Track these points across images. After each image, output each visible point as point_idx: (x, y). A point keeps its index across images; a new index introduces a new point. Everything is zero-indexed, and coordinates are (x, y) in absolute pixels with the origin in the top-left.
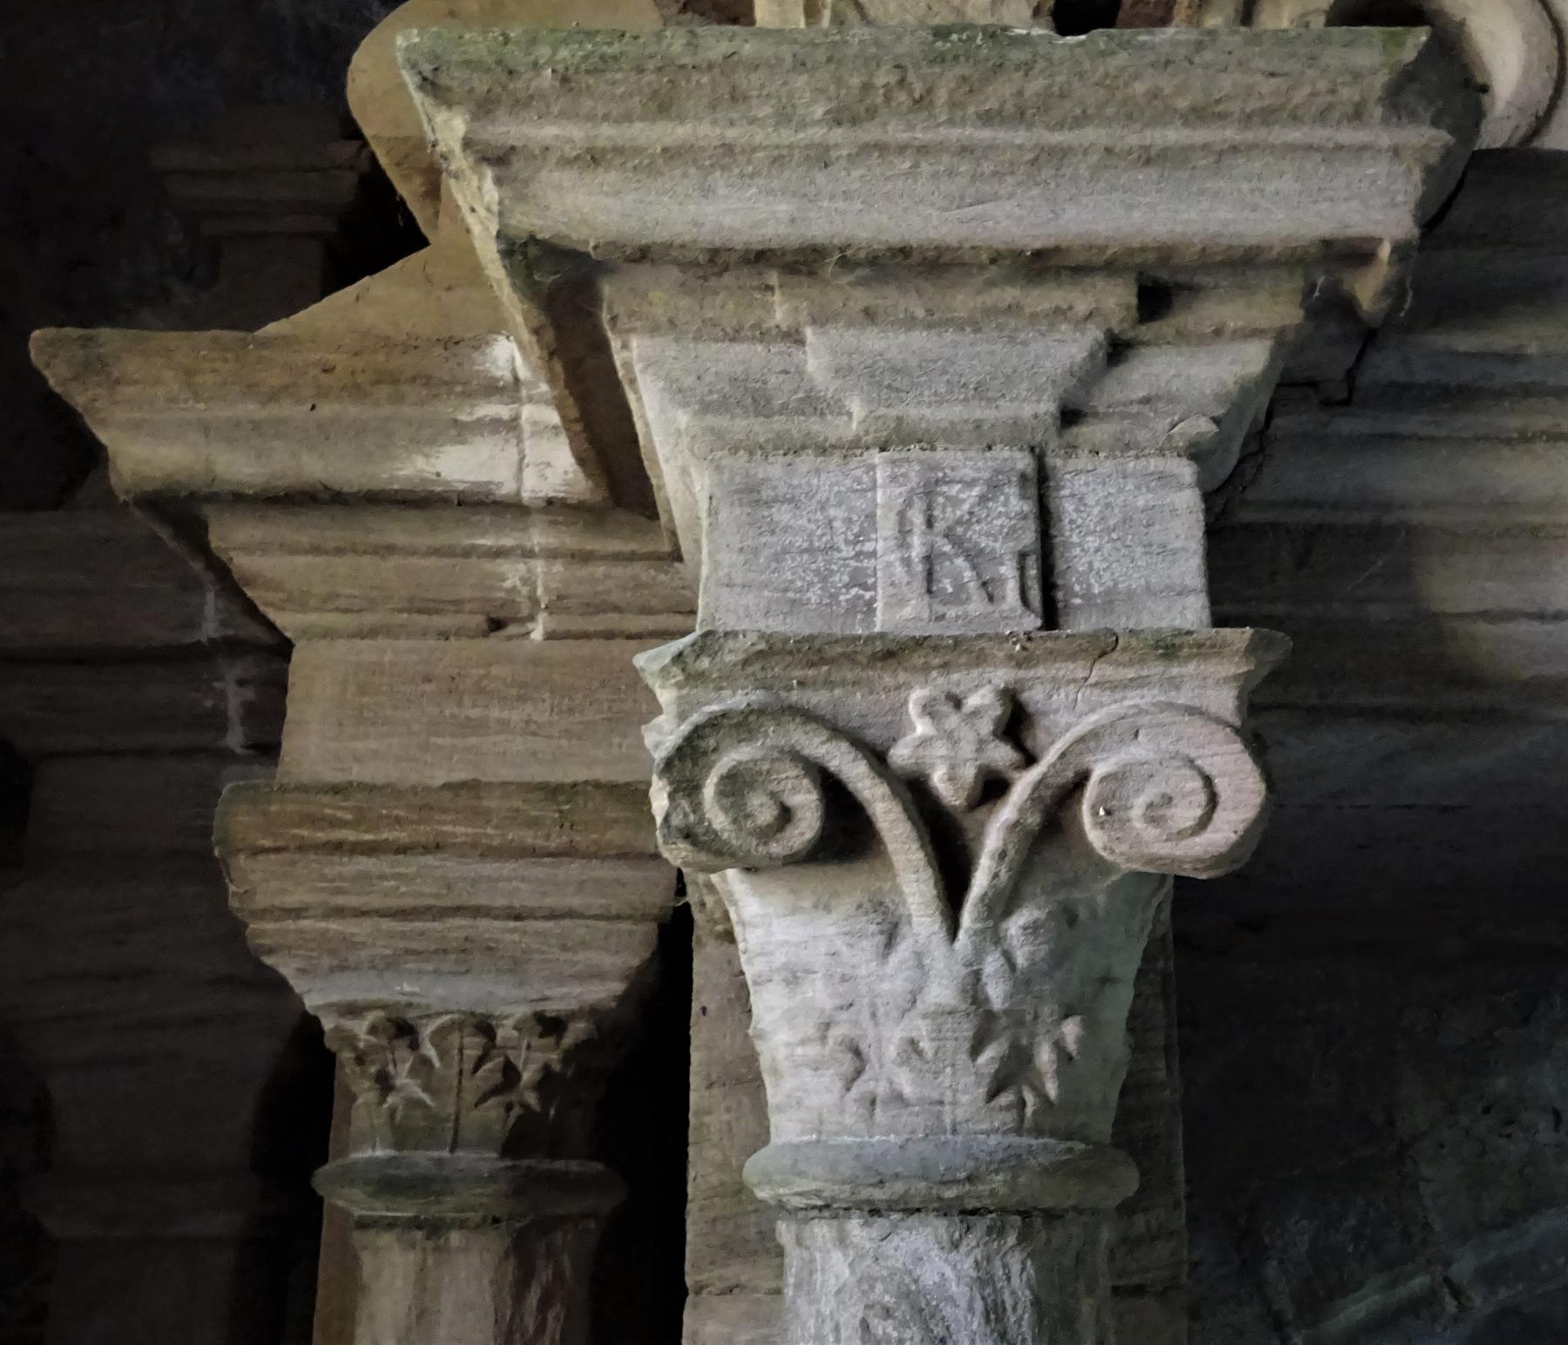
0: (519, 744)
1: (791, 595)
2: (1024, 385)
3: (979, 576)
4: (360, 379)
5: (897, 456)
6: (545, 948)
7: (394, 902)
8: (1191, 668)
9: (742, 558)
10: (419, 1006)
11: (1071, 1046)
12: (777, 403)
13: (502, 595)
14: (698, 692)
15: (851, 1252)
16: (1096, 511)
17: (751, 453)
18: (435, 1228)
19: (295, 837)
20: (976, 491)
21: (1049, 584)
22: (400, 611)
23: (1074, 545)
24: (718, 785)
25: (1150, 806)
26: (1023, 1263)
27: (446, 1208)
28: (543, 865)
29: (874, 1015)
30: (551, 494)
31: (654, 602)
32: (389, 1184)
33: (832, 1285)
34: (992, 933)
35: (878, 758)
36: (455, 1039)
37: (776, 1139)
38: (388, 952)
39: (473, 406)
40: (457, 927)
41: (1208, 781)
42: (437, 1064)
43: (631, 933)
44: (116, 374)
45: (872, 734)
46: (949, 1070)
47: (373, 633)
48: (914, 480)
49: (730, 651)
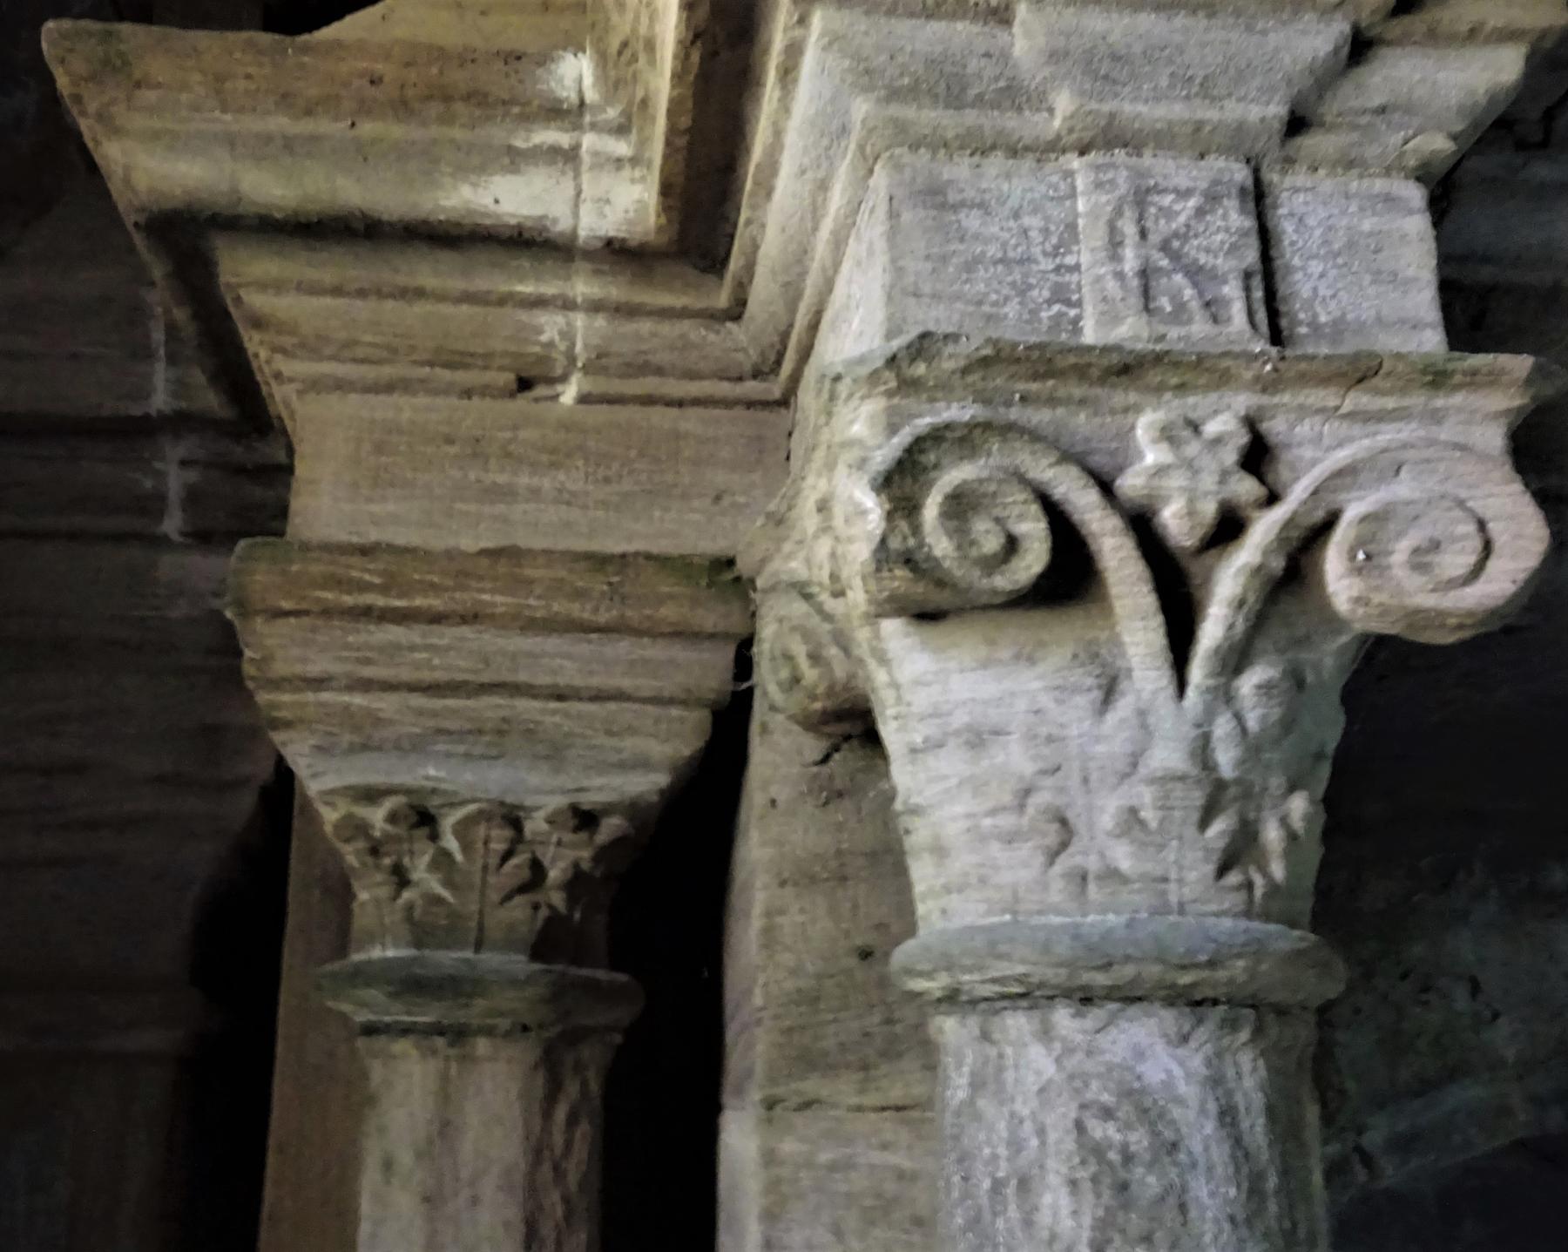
0: (553, 514)
1: (986, 308)
2: (1256, 82)
3: (1201, 294)
4: (410, 92)
5: (1100, 161)
6: (589, 732)
7: (427, 676)
8: (1458, 399)
9: (929, 266)
10: (445, 792)
11: (1298, 824)
12: (972, 92)
13: (537, 349)
14: (909, 403)
15: (1057, 1046)
16: (1318, 232)
17: (934, 153)
18: (458, 1034)
19: (318, 600)
20: (1192, 203)
21: (1273, 314)
22: (422, 364)
23: (1297, 269)
24: (942, 505)
25: (1416, 551)
26: (1255, 1060)
27: (475, 1011)
28: (590, 642)
29: (1086, 780)
30: (612, 234)
31: (702, 365)
32: (412, 984)
33: (1032, 1083)
34: (1223, 694)
35: (1106, 487)
36: (481, 831)
37: (922, 931)
38: (417, 730)
39: (529, 131)
40: (491, 707)
41: (1482, 525)
42: (459, 857)
43: (682, 720)
44: (137, 75)
45: (1098, 461)
46: (1174, 843)
47: (389, 387)
48: (1123, 187)
49: (951, 356)
